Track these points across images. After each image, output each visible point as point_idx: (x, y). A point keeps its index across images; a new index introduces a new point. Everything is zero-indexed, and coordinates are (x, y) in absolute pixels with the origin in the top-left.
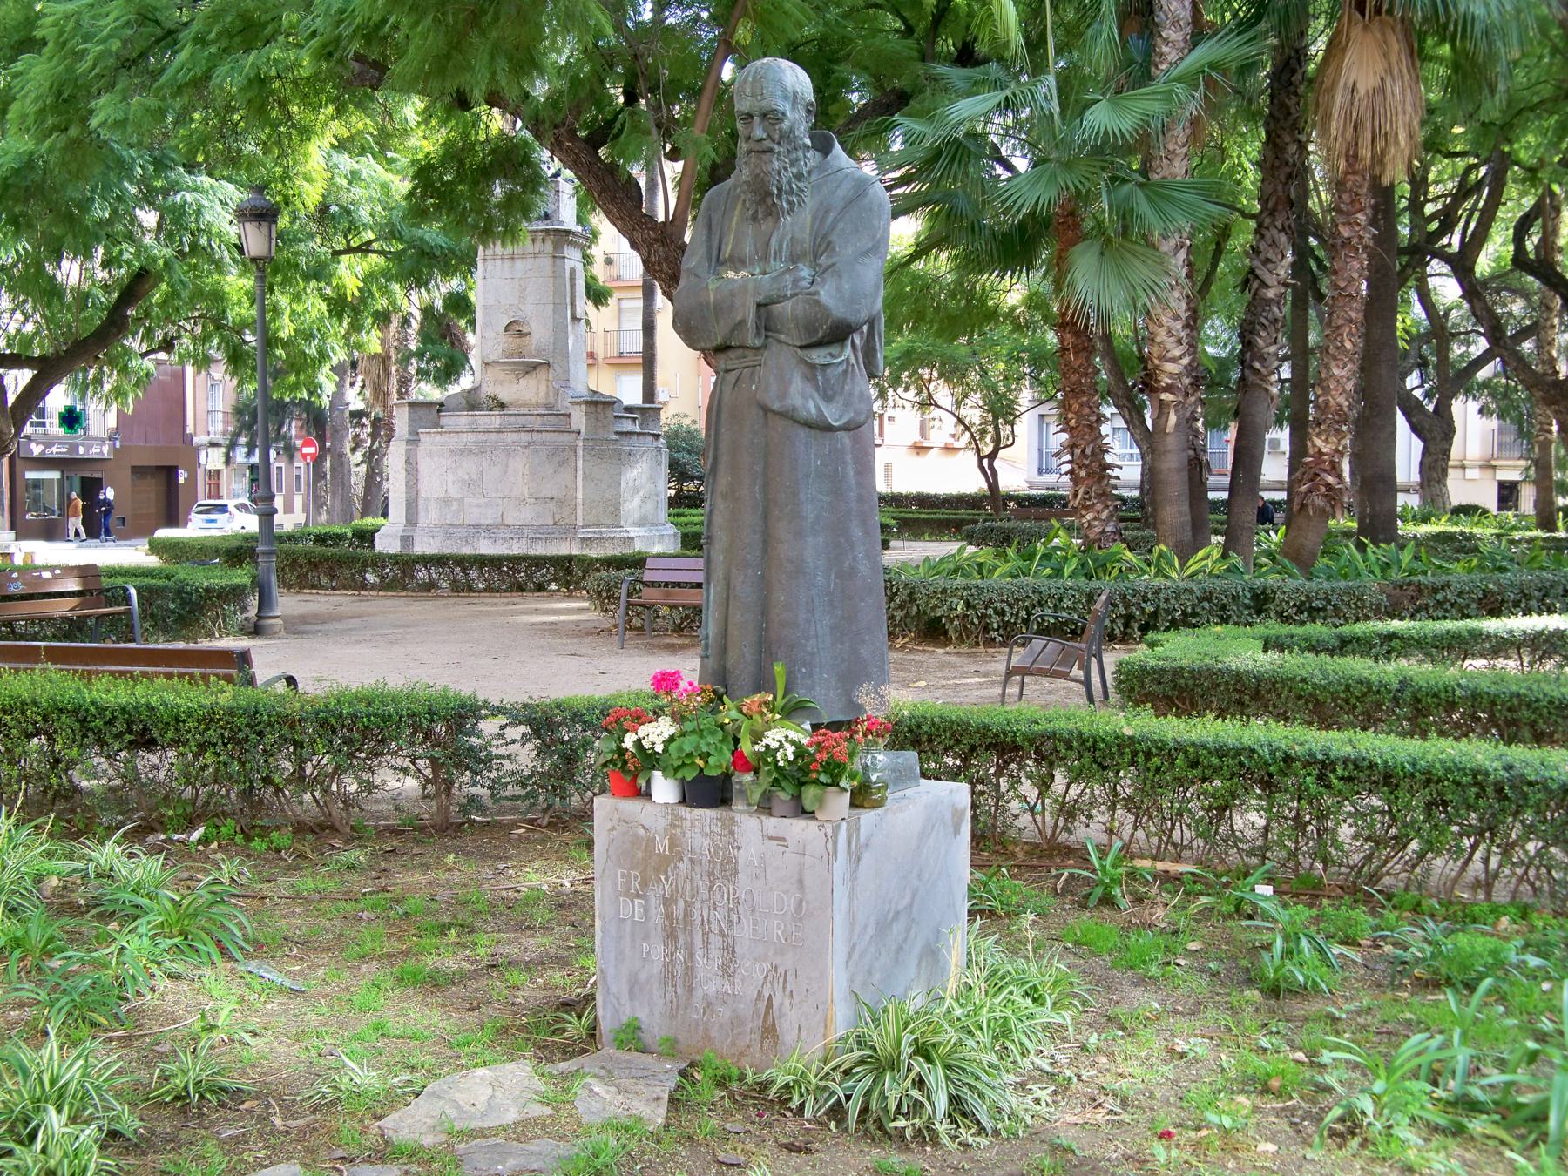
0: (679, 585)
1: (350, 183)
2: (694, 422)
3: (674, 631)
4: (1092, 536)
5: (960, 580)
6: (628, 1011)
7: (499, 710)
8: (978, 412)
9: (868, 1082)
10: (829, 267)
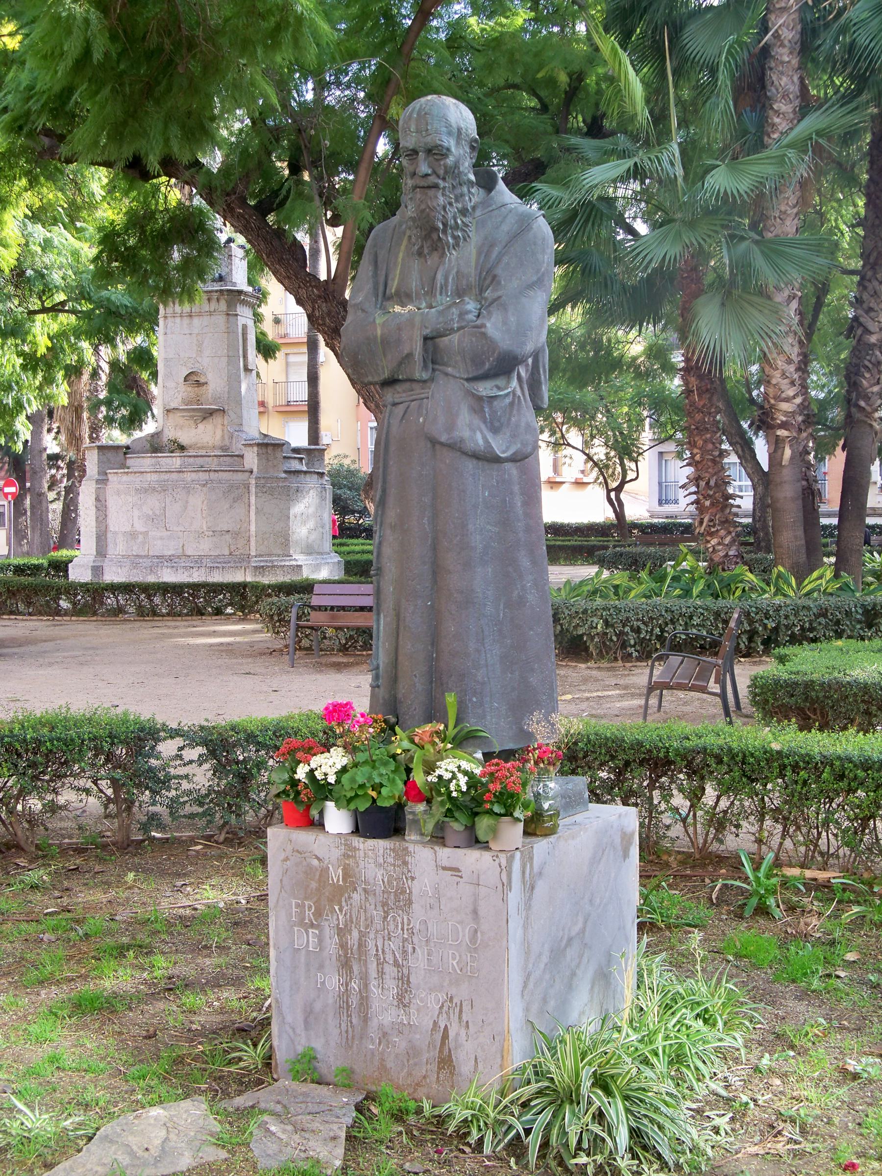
0: (343, 608)
1: (43, 250)
2: (354, 462)
3: (339, 650)
4: (716, 559)
5: (599, 601)
6: (303, 1041)
7: (175, 733)
9: (547, 1115)
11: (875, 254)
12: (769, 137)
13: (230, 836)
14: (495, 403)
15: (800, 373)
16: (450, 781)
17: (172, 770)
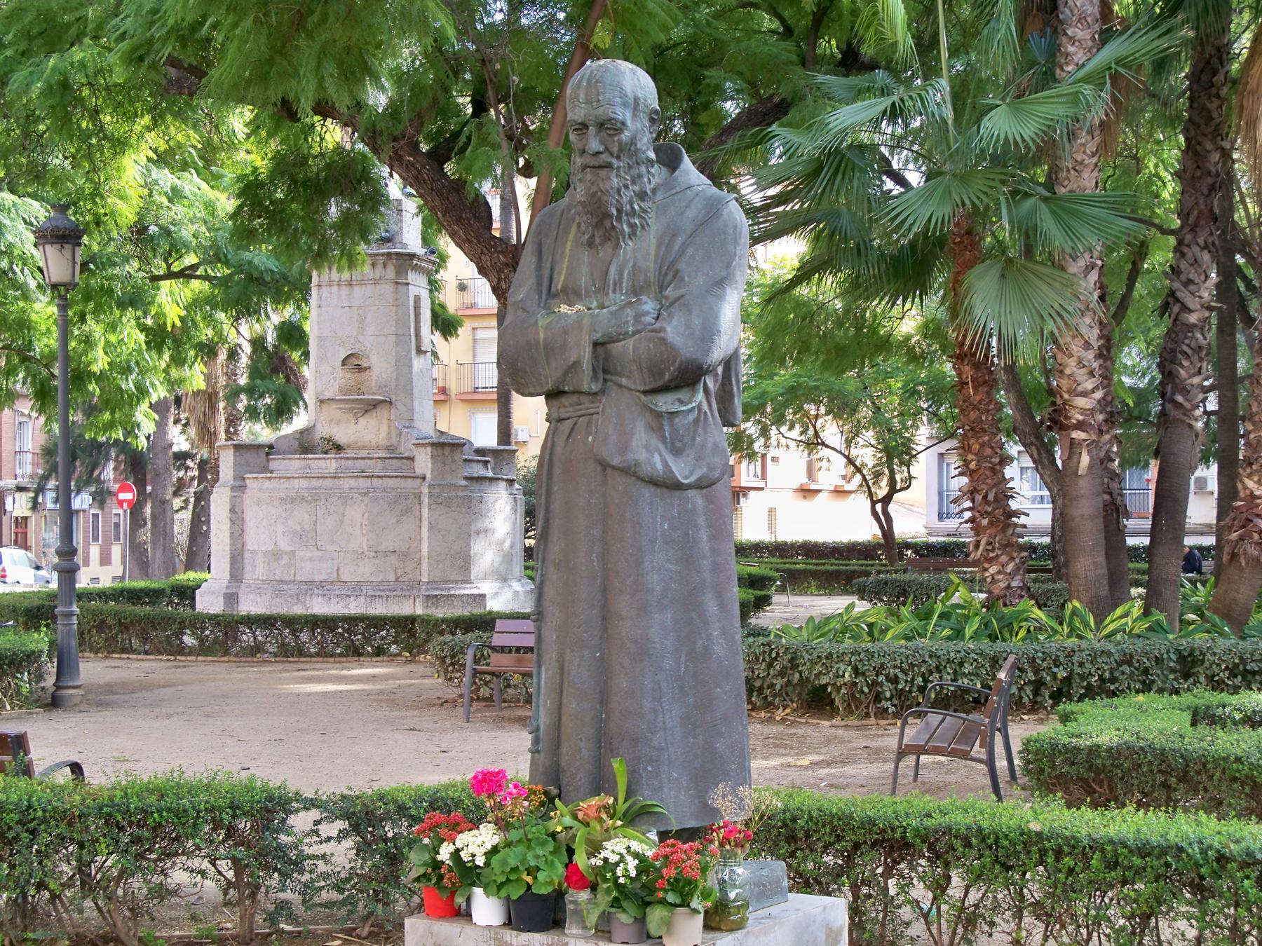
1: (170, 200)
4: (996, 592)
5: (848, 643)
7: (310, 804)
8: (870, 451)
11: (1195, 213)
12: (1062, 70)
13: (376, 929)
14: (677, 420)
15: (1101, 361)
16: (617, 864)
17: (305, 848)
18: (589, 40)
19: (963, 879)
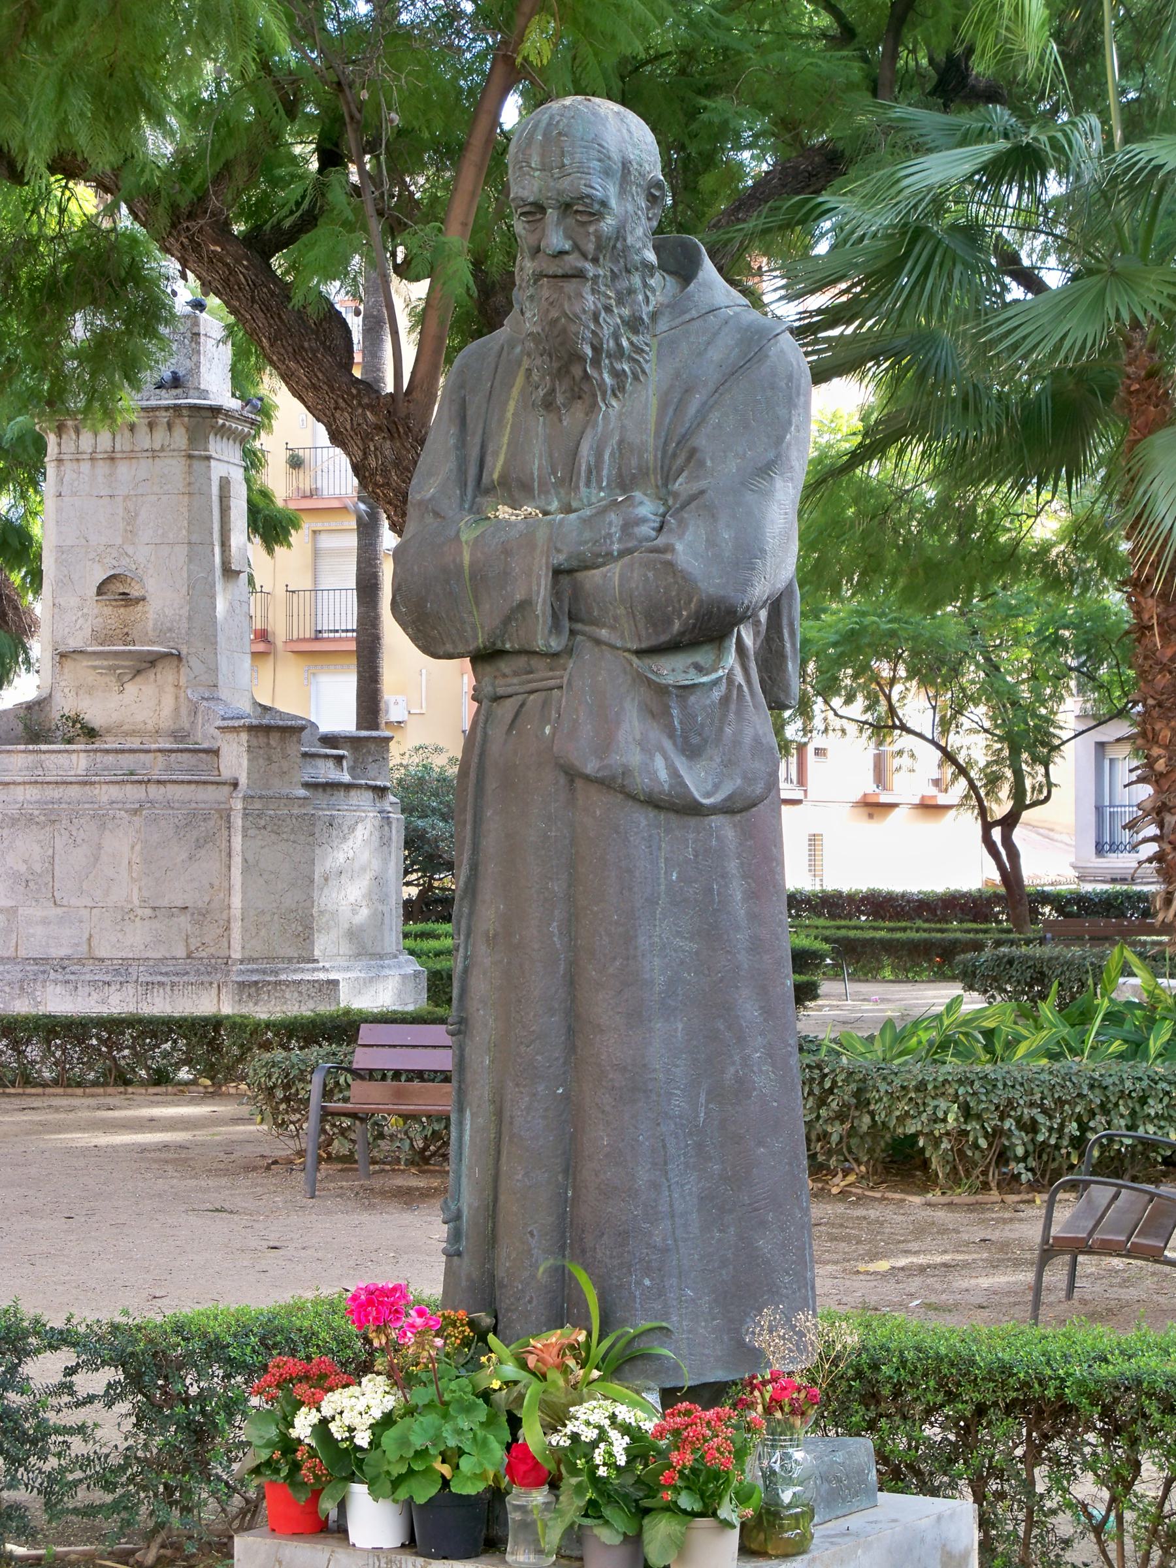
0: (420, 1075)
3: (411, 1163)
5: (952, 1065)
7: (59, 1339)
8: (981, 739)
10: (693, 498)
13: (168, 1552)
16: (594, 1444)
18: (515, 51)
19: (1162, 1469)
